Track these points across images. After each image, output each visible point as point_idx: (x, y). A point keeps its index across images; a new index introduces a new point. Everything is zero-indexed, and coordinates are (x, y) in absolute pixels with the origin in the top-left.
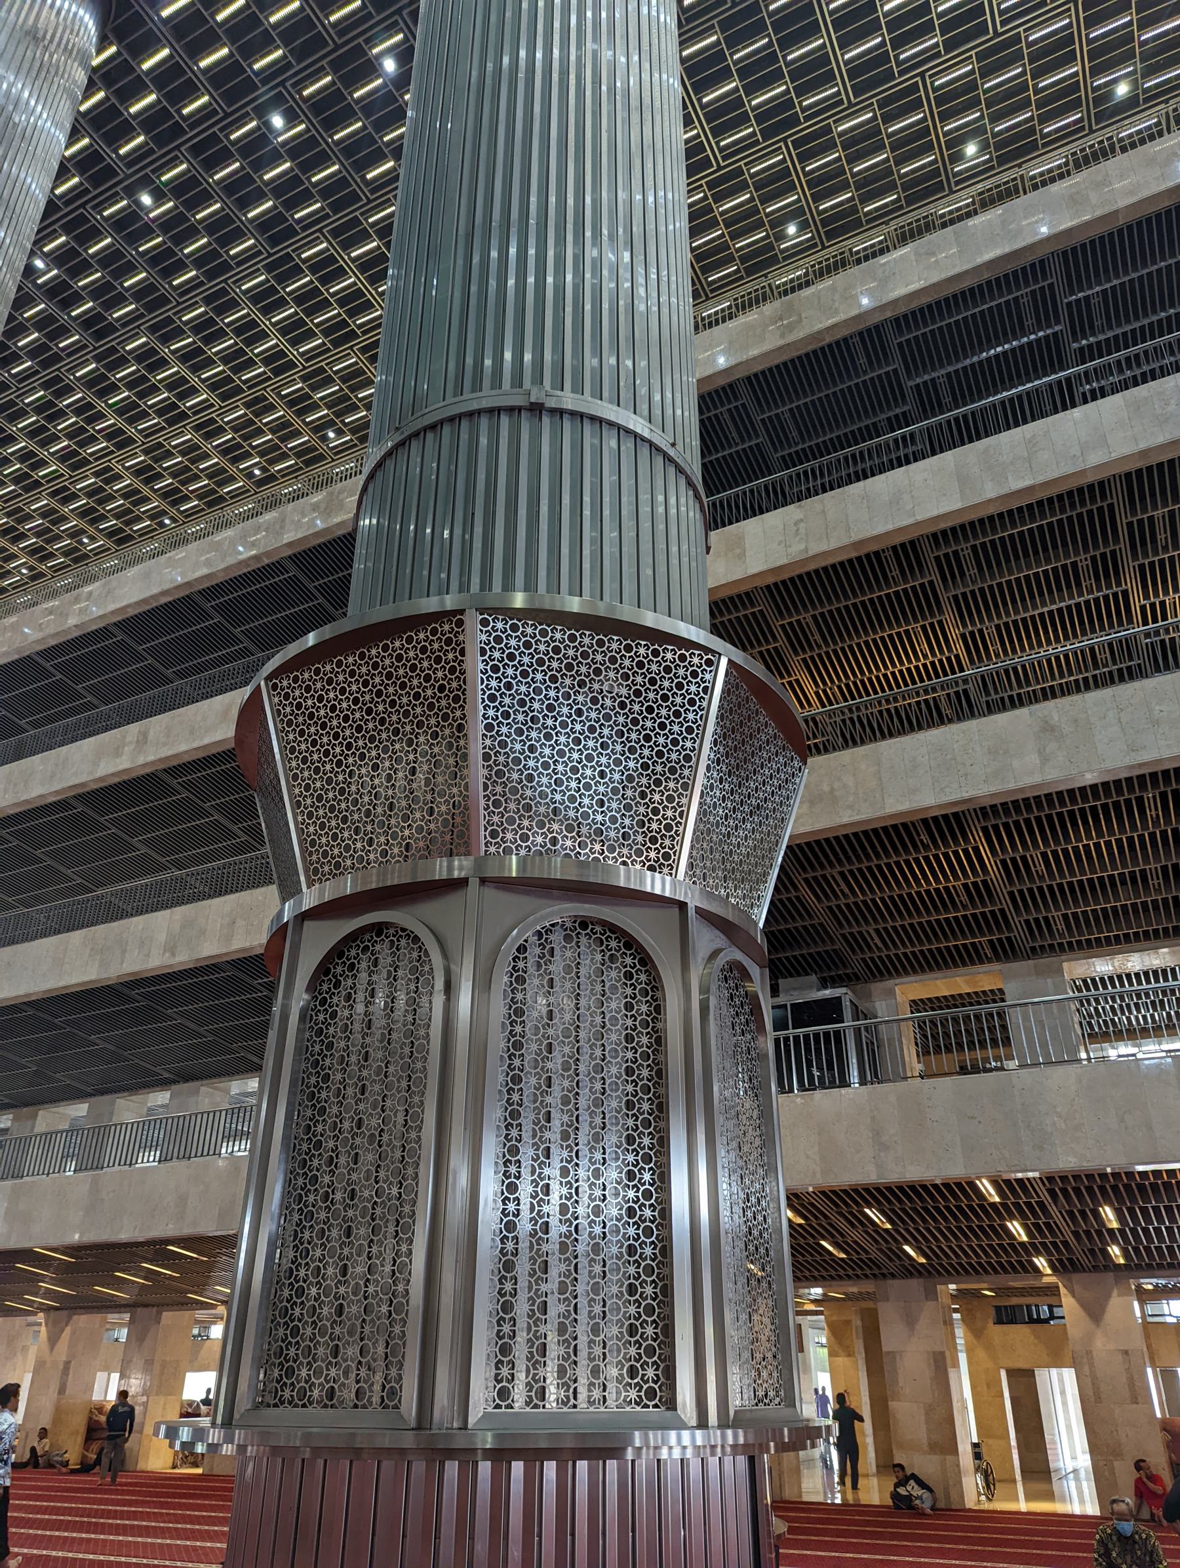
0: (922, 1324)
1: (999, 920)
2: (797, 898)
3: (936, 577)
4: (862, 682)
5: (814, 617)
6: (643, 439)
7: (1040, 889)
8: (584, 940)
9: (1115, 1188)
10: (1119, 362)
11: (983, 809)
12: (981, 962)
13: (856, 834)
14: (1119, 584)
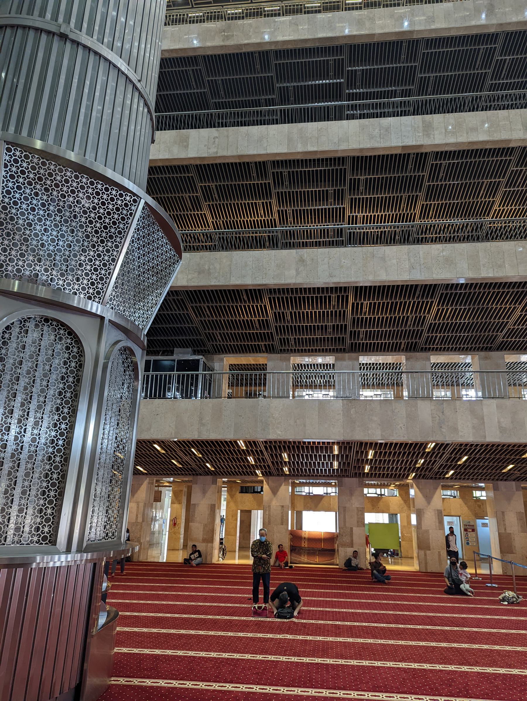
0: (208, 494)
1: (270, 336)
2: (187, 314)
3: (271, 181)
4: (233, 221)
5: (216, 186)
6: (123, 73)
7: (287, 326)
8: (45, 328)
9: (289, 447)
10: (377, 104)
11: (270, 290)
12: (260, 352)
13: (216, 291)
14: (342, 204)
